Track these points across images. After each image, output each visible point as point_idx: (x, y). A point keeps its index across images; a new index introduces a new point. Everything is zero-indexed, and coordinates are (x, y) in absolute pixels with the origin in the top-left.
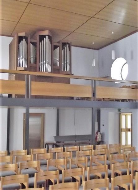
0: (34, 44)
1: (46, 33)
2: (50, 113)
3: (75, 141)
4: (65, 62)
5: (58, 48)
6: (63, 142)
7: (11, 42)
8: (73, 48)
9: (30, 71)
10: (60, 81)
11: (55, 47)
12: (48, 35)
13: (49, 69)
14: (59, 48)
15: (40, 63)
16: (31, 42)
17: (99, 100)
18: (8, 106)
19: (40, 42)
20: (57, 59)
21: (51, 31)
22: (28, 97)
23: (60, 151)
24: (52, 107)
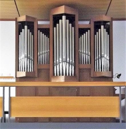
0: (46, 31)
1: (61, 10)
5: (87, 34)
7: (107, 96)
10: (92, 92)
11: (82, 31)
12: (65, 14)
14: (90, 31)
15: (39, 53)
19: (53, 27)
20: (85, 54)
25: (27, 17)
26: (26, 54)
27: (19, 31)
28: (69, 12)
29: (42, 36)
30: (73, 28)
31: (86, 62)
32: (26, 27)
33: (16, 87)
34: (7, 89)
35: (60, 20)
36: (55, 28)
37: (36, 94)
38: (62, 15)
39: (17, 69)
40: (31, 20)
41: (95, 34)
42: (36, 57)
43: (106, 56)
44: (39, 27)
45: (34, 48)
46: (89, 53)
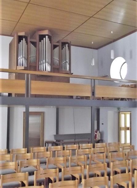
0: (34, 44)
1: (46, 32)
2: (50, 112)
3: (75, 140)
5: (58, 48)
6: (63, 141)
7: (11, 42)
8: (72, 47)
9: (30, 70)
10: (60, 80)
11: (55, 47)
12: (47, 35)
13: (48, 68)
14: (59, 48)
15: (40, 63)
16: (30, 42)
17: (98, 99)
18: (8, 105)
19: (39, 42)
20: (56, 59)
21: (50, 30)
22: (28, 96)
24: (52, 106)
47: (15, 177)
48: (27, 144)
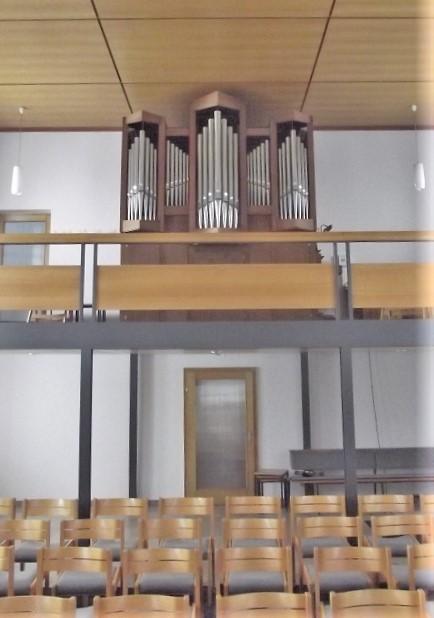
0: (183, 143)
1: (212, 100)
2: (278, 369)
3: (375, 472)
4: (210, 194)
6: (322, 474)
7: (305, 262)
8: (319, 137)
9: (167, 230)
10: (274, 254)
11: (253, 143)
13: (231, 217)
14: (269, 142)
16: (168, 138)
17: (405, 317)
18: (132, 348)
20: (260, 184)
21: (231, 91)
22: (345, 315)
23: (333, 509)
24: (212, 349)
25: (145, 114)
26: (141, 184)
27: (128, 142)
28: (230, 104)
29: (174, 151)
30: (236, 135)
31: (262, 203)
32: (142, 133)
33: (121, 243)
34: (89, 248)
35: (210, 121)
36: (200, 136)
37: (162, 260)
38: (214, 109)
39: (124, 215)
40: (154, 121)
41: (279, 146)
42: (161, 191)
43: (302, 188)
44: (169, 134)
45: (159, 173)
46: (268, 183)
47: (347, 559)
48: (202, 474)
